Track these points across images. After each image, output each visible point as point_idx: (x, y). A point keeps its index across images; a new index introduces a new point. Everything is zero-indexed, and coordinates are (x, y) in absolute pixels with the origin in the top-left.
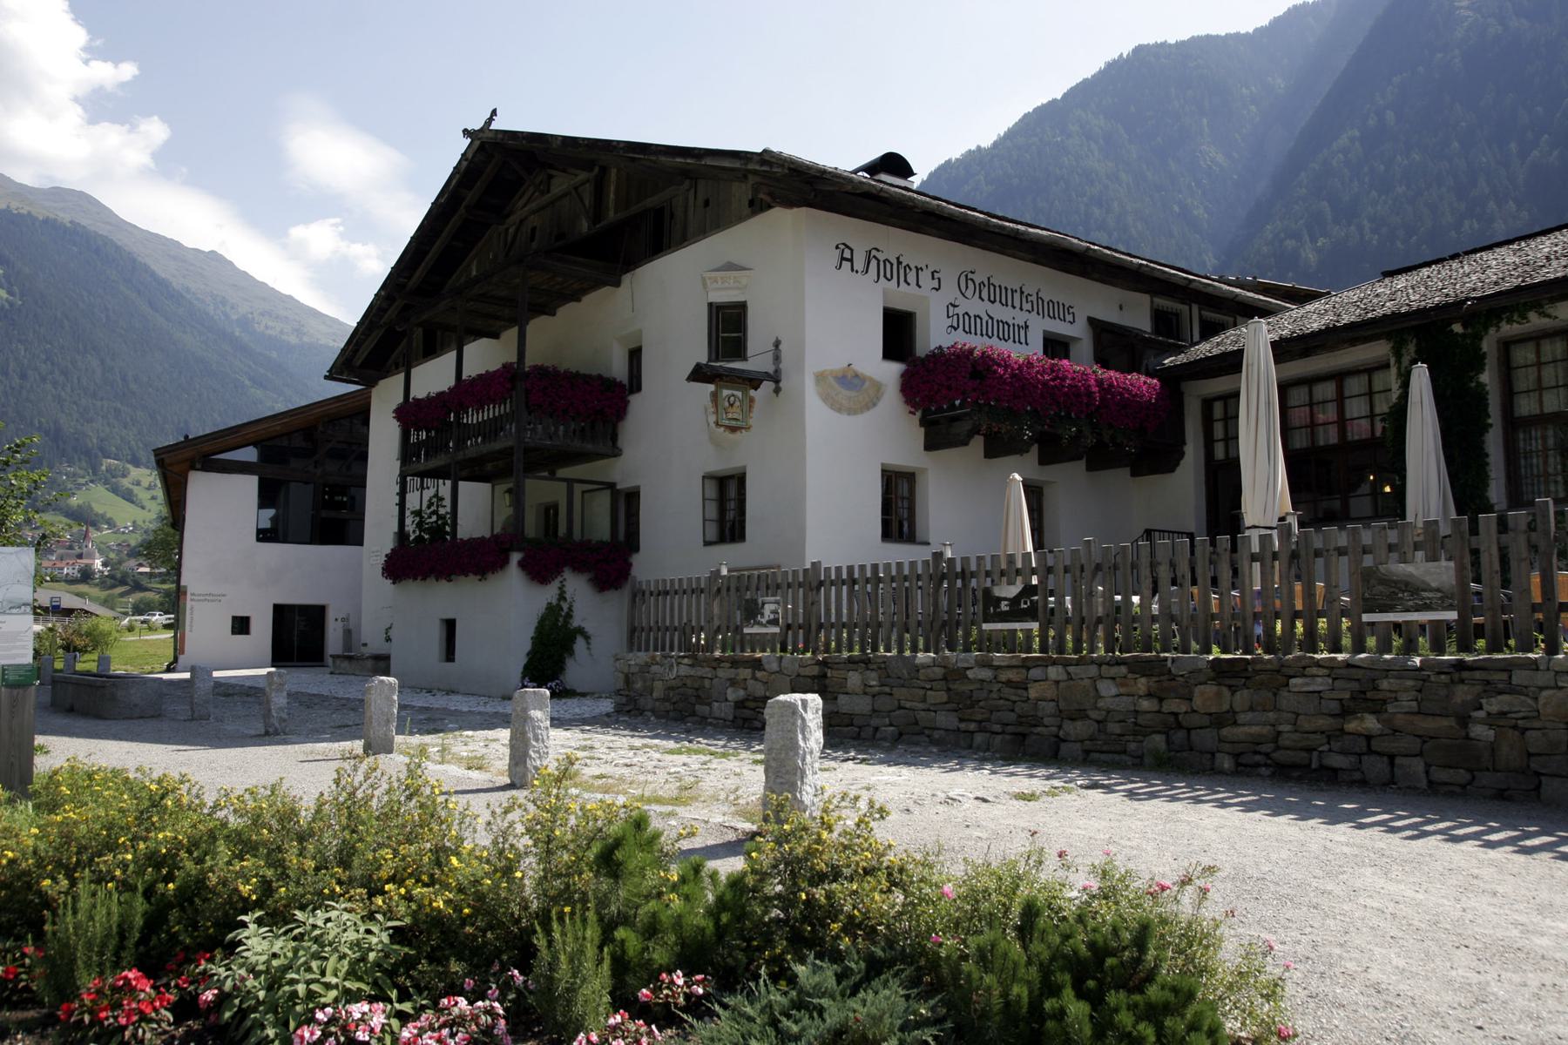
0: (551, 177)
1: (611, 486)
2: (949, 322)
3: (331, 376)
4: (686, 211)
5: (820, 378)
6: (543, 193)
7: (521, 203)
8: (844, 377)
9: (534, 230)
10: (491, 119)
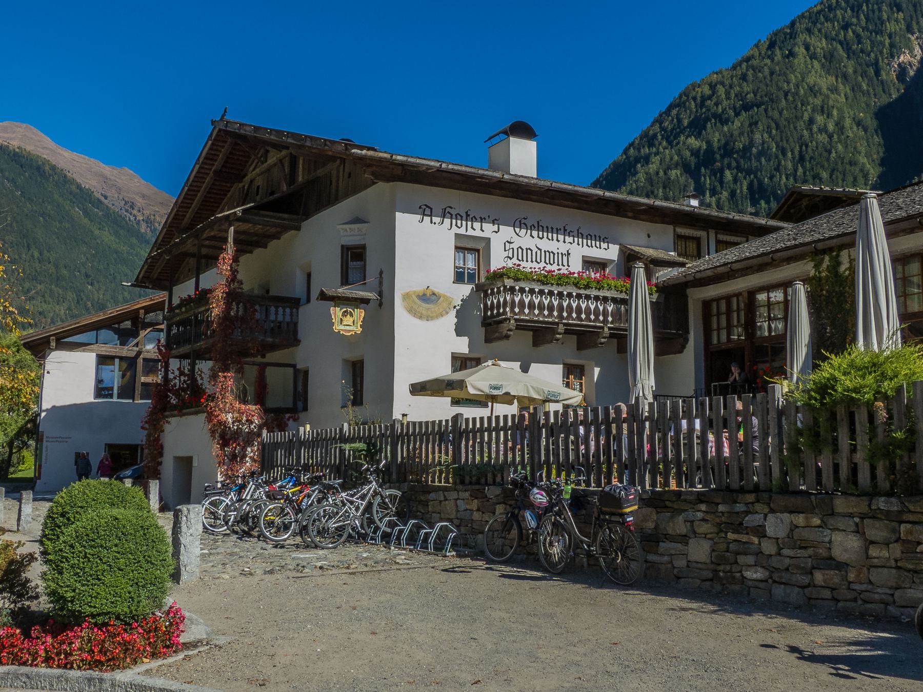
0: (268, 151)
1: (293, 366)
2: (506, 254)
3: (140, 283)
4: (338, 181)
5: (406, 297)
6: (263, 163)
7: (251, 168)
8: (424, 295)
9: (258, 187)
10: (224, 115)
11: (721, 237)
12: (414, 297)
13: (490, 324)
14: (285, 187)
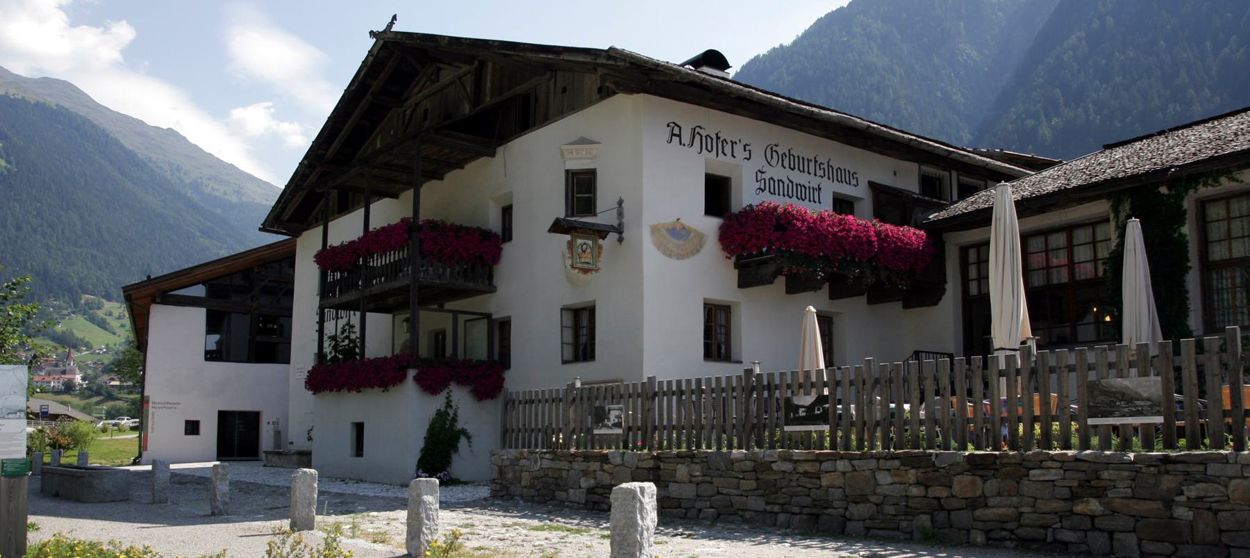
0: (440, 69)
5: (655, 230)
6: (433, 82)
8: (674, 229)
9: (426, 111)
10: (392, 23)
11: (965, 179)
12: (664, 231)
13: (747, 265)
14: (466, 108)
